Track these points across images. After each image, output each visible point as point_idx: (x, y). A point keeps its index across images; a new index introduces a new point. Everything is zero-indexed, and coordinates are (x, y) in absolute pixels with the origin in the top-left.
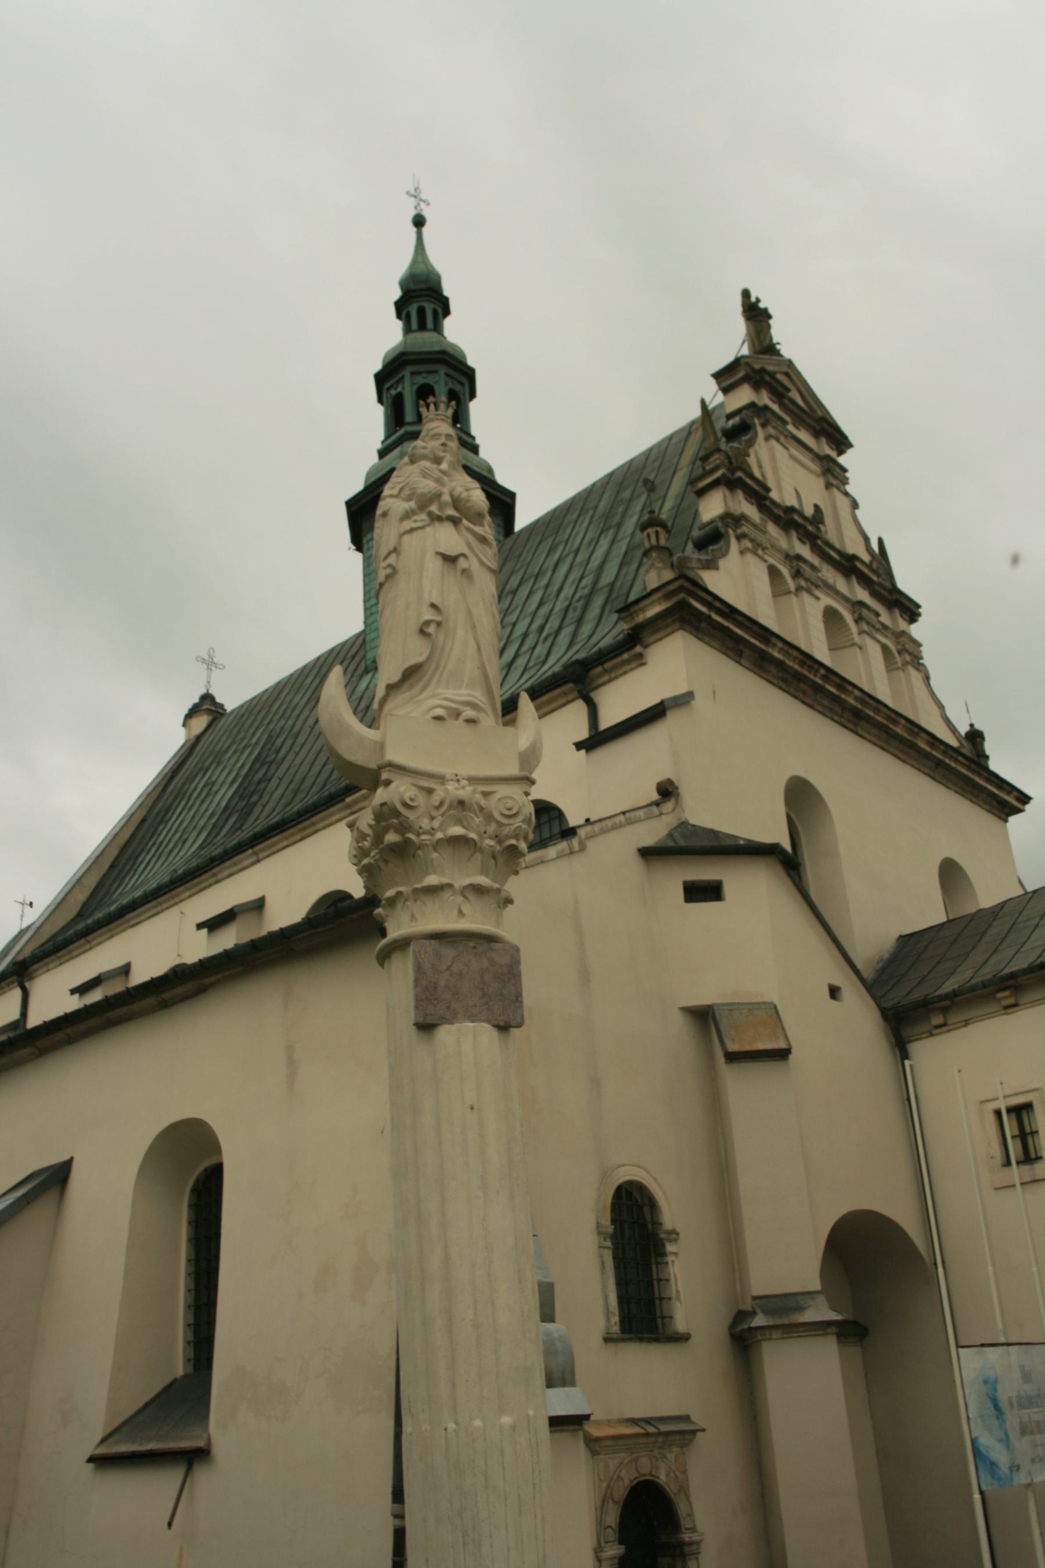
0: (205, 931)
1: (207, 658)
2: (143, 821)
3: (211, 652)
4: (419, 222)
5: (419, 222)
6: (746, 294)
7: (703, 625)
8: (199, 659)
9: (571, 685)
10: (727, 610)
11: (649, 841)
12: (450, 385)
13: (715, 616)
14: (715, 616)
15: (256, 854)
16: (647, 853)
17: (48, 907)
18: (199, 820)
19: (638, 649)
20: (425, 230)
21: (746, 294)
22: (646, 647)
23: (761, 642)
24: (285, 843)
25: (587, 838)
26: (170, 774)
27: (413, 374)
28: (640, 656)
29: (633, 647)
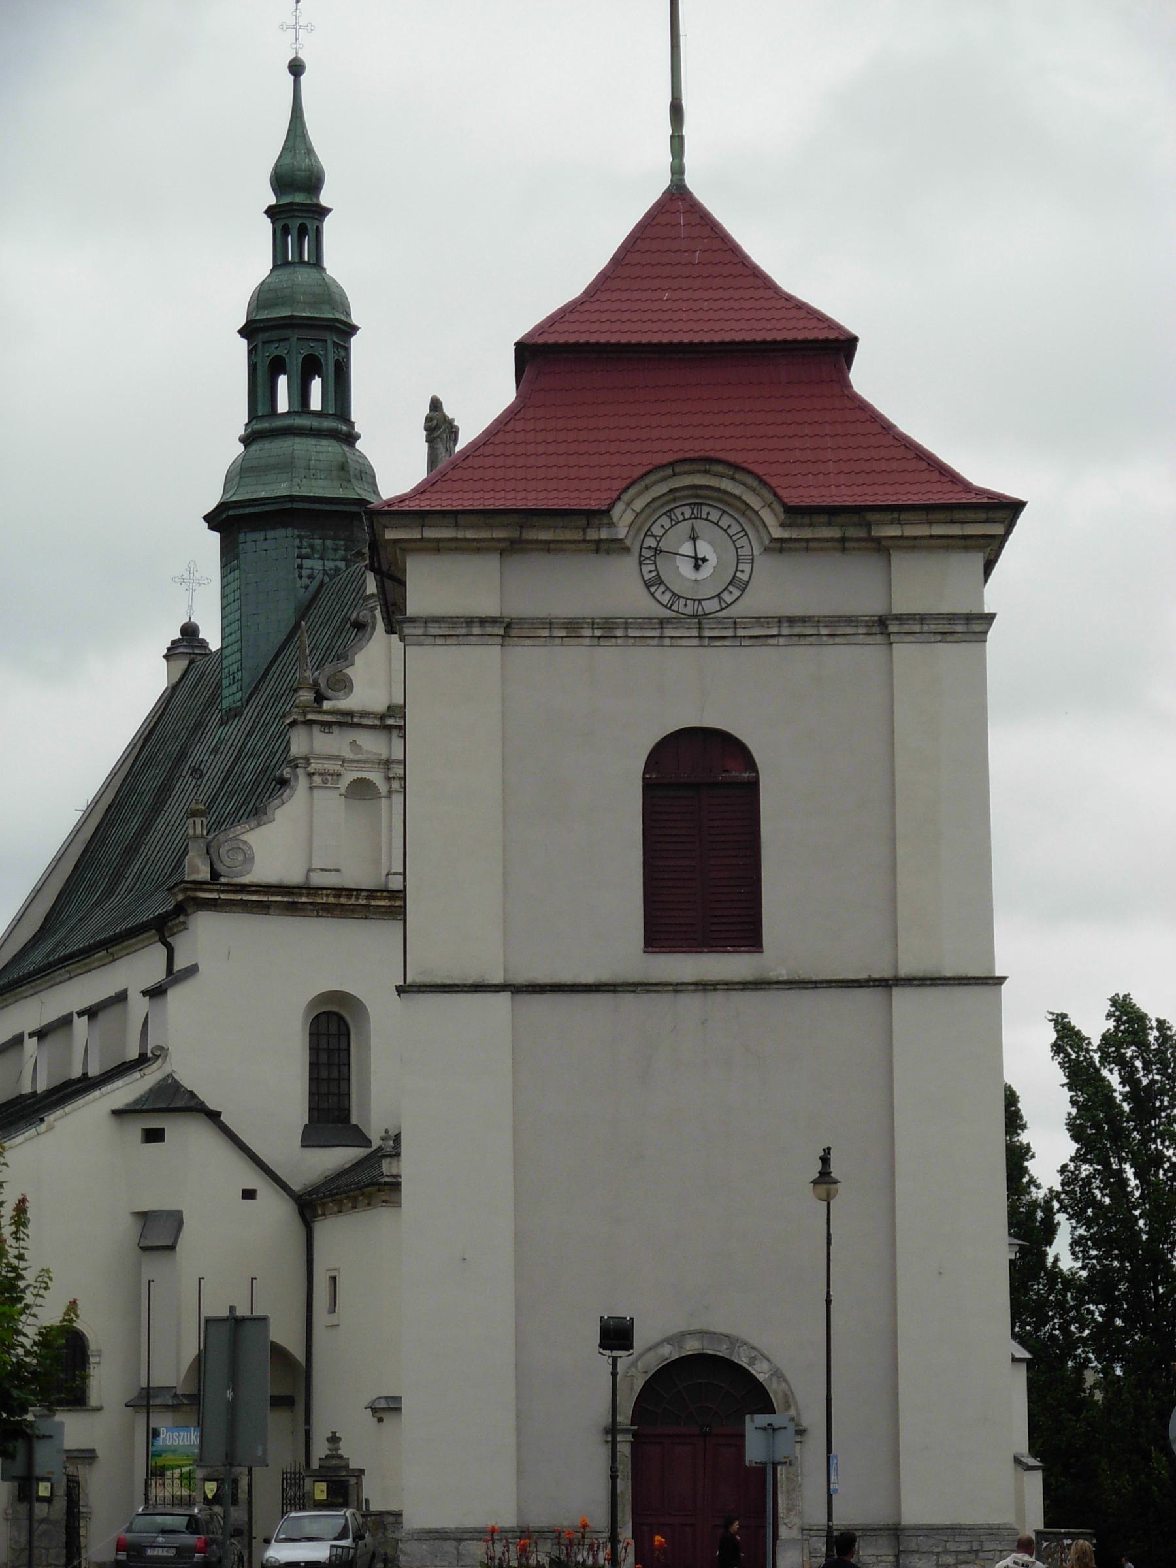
0: (36, 1039)
1: (186, 575)
2: (110, 806)
3: (192, 565)
4: (296, 68)
5: (296, 68)
6: (435, 405)
7: (219, 902)
8: (176, 580)
9: (154, 931)
10: (238, 888)
11: (119, 1104)
12: (305, 352)
13: (223, 896)
14: (223, 896)
15: (69, 972)
16: (116, 1113)
17: (37, 892)
18: (352, 613)
19: (182, 918)
20: (303, 79)
21: (435, 405)
22: (187, 915)
23: (283, 896)
24: (79, 971)
25: (55, 1121)
26: (141, 742)
27: (264, 343)
28: (184, 923)
29: (178, 916)
